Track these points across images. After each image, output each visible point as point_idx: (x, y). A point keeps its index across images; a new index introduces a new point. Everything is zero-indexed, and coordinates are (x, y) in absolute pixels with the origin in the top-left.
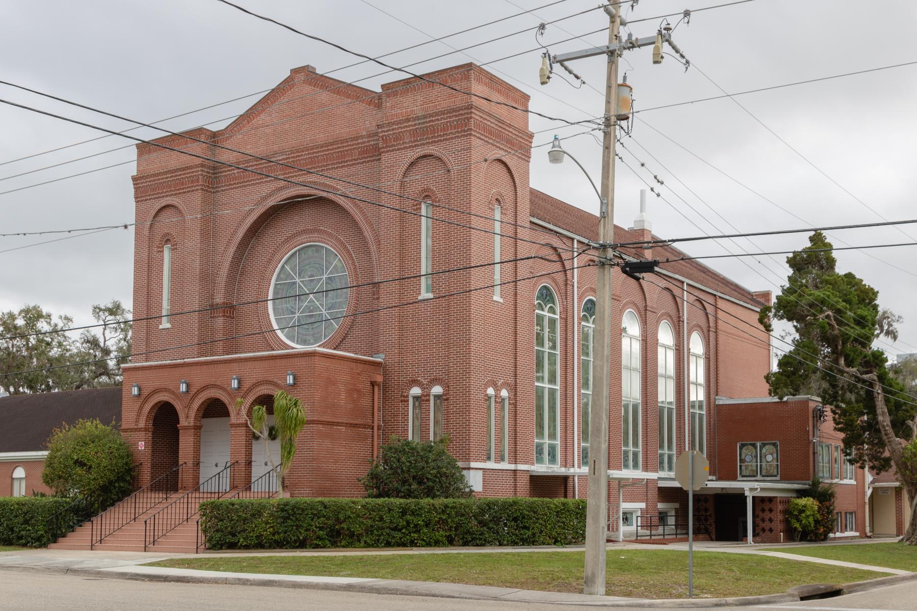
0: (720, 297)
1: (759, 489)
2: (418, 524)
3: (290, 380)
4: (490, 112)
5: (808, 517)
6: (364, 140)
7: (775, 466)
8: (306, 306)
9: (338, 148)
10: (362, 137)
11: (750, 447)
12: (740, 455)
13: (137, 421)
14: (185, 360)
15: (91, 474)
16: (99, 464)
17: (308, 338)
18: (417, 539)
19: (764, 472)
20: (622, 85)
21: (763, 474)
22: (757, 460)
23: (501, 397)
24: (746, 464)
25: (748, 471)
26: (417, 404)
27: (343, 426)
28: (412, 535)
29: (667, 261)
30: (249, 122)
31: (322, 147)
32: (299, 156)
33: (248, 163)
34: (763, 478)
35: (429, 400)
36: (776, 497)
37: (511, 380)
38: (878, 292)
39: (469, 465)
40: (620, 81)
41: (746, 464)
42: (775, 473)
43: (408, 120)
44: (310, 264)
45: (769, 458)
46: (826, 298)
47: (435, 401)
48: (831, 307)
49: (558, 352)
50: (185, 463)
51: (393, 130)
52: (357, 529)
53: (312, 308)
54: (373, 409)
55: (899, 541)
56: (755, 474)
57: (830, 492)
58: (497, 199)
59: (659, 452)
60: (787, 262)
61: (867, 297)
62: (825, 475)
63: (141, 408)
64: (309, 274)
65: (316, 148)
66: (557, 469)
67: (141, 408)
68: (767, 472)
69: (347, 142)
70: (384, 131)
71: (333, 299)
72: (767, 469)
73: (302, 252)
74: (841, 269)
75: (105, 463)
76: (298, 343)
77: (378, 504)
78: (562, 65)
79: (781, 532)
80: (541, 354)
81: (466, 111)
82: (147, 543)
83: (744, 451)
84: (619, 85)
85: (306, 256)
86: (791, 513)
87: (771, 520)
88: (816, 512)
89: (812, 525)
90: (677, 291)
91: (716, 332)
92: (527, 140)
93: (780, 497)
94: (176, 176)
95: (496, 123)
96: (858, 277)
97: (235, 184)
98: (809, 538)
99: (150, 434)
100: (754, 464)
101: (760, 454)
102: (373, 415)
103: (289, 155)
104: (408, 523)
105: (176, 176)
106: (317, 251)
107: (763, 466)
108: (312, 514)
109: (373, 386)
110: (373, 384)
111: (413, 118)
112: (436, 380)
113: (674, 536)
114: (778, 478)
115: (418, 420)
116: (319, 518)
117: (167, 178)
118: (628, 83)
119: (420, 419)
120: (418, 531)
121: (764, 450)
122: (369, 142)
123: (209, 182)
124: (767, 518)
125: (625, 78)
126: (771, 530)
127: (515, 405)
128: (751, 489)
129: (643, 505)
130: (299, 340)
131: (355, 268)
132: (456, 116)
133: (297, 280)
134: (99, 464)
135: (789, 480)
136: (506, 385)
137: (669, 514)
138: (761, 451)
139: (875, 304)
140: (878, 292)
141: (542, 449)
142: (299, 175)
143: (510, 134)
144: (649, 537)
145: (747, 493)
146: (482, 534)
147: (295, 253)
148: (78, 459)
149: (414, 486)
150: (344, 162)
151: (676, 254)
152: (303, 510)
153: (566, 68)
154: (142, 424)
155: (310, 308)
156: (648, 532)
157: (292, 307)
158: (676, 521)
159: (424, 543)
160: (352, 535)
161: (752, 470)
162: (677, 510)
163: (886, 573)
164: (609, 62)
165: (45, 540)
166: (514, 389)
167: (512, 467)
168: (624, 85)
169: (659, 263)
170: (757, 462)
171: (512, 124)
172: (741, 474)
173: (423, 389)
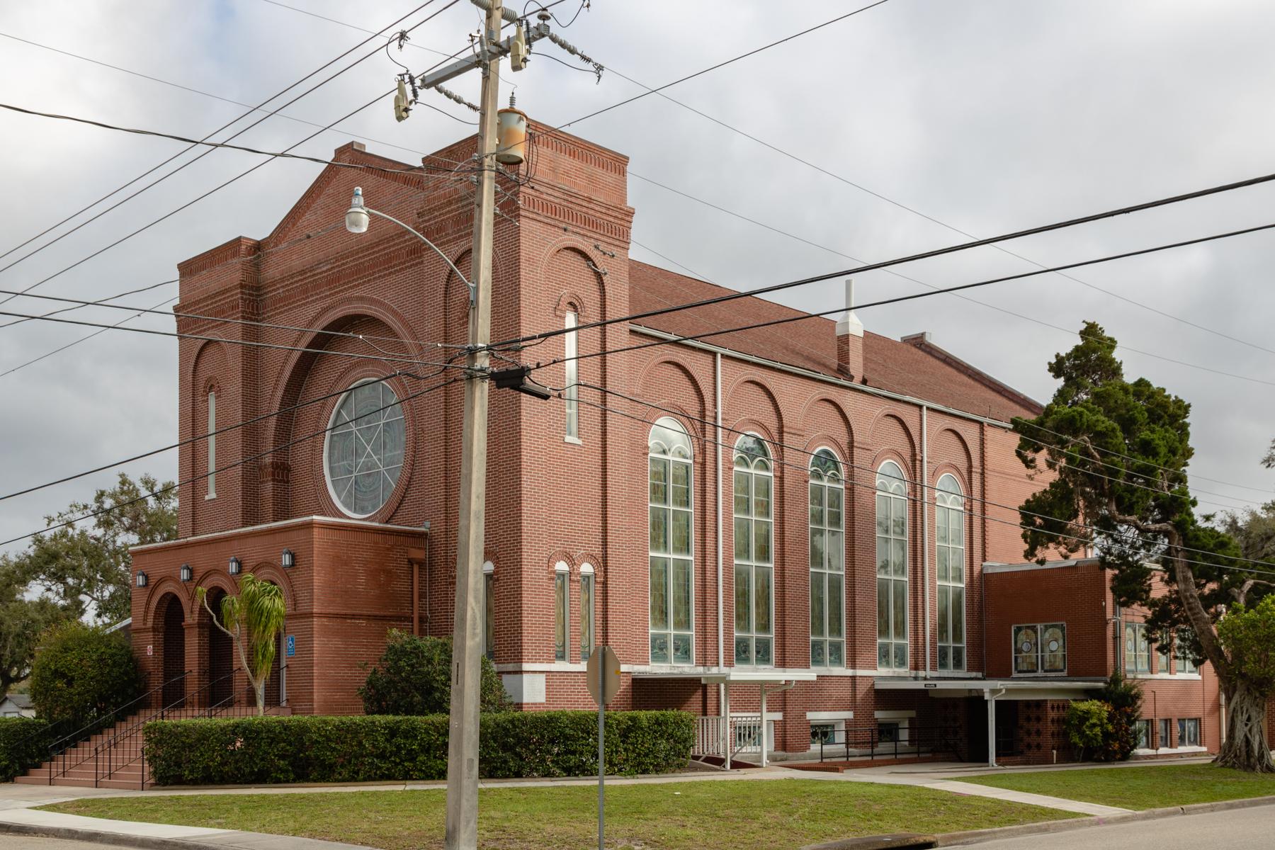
0: (989, 425)
1: (1004, 691)
2: (412, 750)
3: (286, 560)
4: (552, 183)
5: (1094, 725)
9: (384, 249)
11: (1030, 632)
13: (145, 620)
14: (188, 539)
15: (72, 687)
16: (84, 675)
17: (366, 504)
18: (412, 770)
19: (1047, 666)
20: (506, 111)
22: (1037, 649)
23: (579, 574)
24: (1024, 654)
27: (363, 619)
28: (406, 764)
29: (538, 366)
30: (294, 225)
31: (367, 250)
32: (343, 264)
33: (292, 278)
34: (1021, 675)
36: (1046, 701)
37: (597, 551)
38: (1189, 406)
39: (521, 667)
40: (503, 104)
41: (1024, 654)
42: (1062, 667)
43: (450, 203)
45: (1054, 646)
46: (1078, 417)
48: (1089, 429)
50: (191, 671)
51: (435, 218)
52: (329, 756)
53: (370, 464)
54: (412, 594)
55: (1213, 762)
56: (1035, 669)
57: (1133, 692)
59: (879, 641)
60: (1050, 370)
61: (1166, 413)
62: (1139, 667)
63: (148, 603)
65: (362, 252)
66: (689, 669)
67: (148, 603)
69: (394, 239)
70: (425, 221)
71: (391, 451)
72: (1050, 662)
74: (1129, 377)
75: (92, 672)
76: (355, 512)
77: (355, 723)
78: (440, 90)
79: (1054, 749)
80: (661, 513)
82: (100, 776)
83: (1022, 636)
84: (501, 113)
86: (1072, 722)
87: (1038, 733)
88: (1105, 721)
89: (1099, 739)
90: (909, 416)
91: (983, 474)
92: (622, 219)
93: (1050, 700)
94: (216, 302)
95: (565, 197)
96: (1155, 385)
97: (280, 307)
98: (1095, 757)
99: (161, 636)
100: (1034, 655)
102: (413, 603)
103: (334, 263)
104: (399, 748)
105: (216, 302)
107: (1045, 658)
108: (268, 737)
109: (412, 565)
110: (411, 562)
111: (454, 199)
113: (916, 756)
116: (278, 743)
117: (207, 305)
118: (517, 107)
120: (413, 760)
121: (1047, 635)
123: (253, 307)
125: (512, 100)
126: (1038, 746)
127: (605, 584)
128: (994, 691)
129: (849, 715)
130: (357, 507)
133: (354, 429)
134: (84, 675)
136: (590, 557)
137: (900, 726)
139: (1184, 423)
140: (1189, 406)
142: (345, 289)
143: (591, 212)
145: (987, 697)
146: (506, 762)
148: (56, 670)
149: (418, 698)
150: (392, 267)
151: (963, 369)
152: (258, 733)
153: (449, 95)
154: (150, 624)
157: (349, 465)
158: (911, 735)
159: (422, 775)
160: (322, 764)
161: (1032, 663)
162: (911, 720)
163: (1074, 813)
164: (483, 78)
165: (10, 772)
166: (604, 562)
168: (511, 111)
169: (530, 370)
170: (1037, 652)
171: (593, 197)
172: (1016, 668)
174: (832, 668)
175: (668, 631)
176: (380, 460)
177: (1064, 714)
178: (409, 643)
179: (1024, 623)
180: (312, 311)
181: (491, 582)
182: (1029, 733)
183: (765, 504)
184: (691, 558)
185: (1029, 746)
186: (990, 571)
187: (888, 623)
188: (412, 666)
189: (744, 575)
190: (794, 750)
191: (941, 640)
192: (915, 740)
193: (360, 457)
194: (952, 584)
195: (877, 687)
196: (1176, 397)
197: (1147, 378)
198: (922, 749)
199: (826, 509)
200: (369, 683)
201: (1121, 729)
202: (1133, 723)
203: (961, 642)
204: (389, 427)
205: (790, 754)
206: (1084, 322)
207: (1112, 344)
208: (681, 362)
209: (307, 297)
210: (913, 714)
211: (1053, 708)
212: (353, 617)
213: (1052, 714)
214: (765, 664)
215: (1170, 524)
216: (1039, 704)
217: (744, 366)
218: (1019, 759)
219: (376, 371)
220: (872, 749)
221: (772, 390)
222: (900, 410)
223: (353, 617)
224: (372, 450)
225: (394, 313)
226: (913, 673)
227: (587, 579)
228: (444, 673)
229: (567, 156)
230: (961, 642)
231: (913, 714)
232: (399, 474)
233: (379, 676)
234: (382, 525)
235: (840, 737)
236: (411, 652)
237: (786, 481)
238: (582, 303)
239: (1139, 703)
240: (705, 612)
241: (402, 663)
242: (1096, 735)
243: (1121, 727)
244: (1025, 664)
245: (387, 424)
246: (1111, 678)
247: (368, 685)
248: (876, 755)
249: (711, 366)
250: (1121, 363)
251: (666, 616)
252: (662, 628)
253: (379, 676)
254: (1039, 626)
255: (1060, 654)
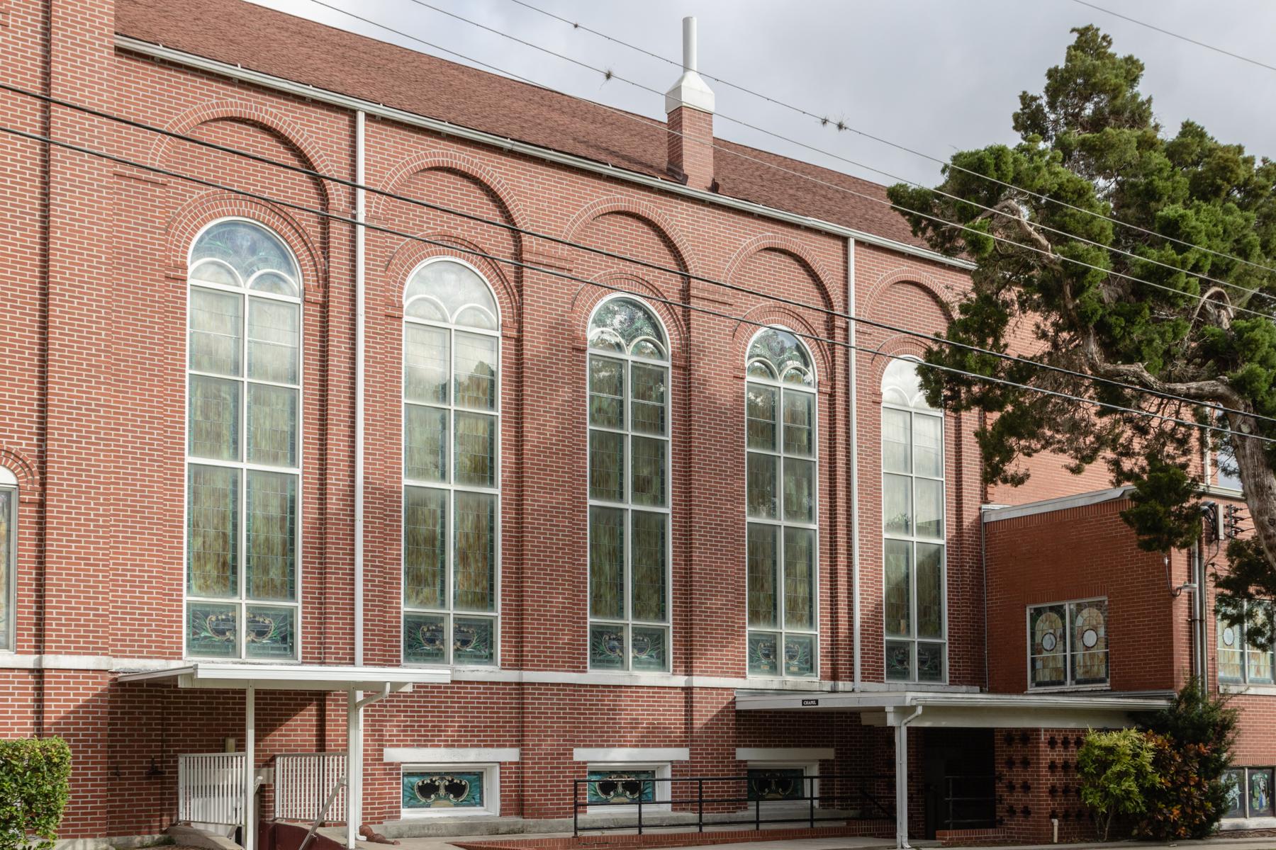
1: (919, 711)
5: (1121, 776)
7: (1102, 656)
11: (1054, 616)
12: (1033, 635)
19: (1080, 674)
21: (1078, 677)
24: (1045, 654)
25: (1047, 672)
34: (1041, 689)
36: (1038, 730)
41: (1045, 654)
42: (1103, 675)
45: (1090, 638)
49: (668, 437)
62: (1252, 675)
68: (1087, 672)
72: (1085, 666)
83: (1042, 625)
87: (1026, 787)
90: (823, 255)
93: (1046, 730)
98: (1135, 832)
100: (1060, 655)
101: (1072, 629)
113: (807, 825)
114: (1106, 686)
124: (1018, 782)
126: (1026, 812)
128: (904, 711)
129: (682, 754)
135: (1130, 690)
138: (1072, 622)
144: (695, 829)
156: (691, 816)
158: (823, 788)
161: (1056, 669)
162: (824, 764)
167: (512, 676)
172: (1033, 679)
174: (637, 673)
175: (235, 600)
177: (1074, 754)
179: (1044, 602)
182: (1011, 787)
183: (486, 384)
184: (298, 471)
185: (1011, 811)
186: (993, 518)
187: (775, 600)
189: (432, 506)
190: (540, 813)
191: (893, 629)
192: (833, 799)
194: (916, 539)
195: (739, 707)
196: (1264, 161)
197: (1199, 123)
198: (707, 816)
199: (629, 398)
201: (1186, 784)
202: (1217, 772)
203: (940, 636)
205: (531, 821)
206: (1073, 30)
207: (1132, 70)
208: (268, 120)
210: (829, 753)
211: (1052, 743)
213: (1048, 755)
214: (486, 663)
215: (1223, 382)
216: (1027, 736)
217: (429, 140)
218: (990, 833)
220: (701, 814)
221: (495, 185)
222: (796, 241)
226: (828, 685)
230: (940, 636)
231: (829, 753)
235: (664, 791)
237: (527, 345)
239: (1230, 735)
240: (323, 566)
242: (1128, 792)
243: (1187, 779)
244: (1047, 672)
246: (1183, 692)
248: (707, 824)
249: (345, 134)
250: (1149, 101)
252: (224, 595)
254: (1069, 606)
255: (1101, 651)
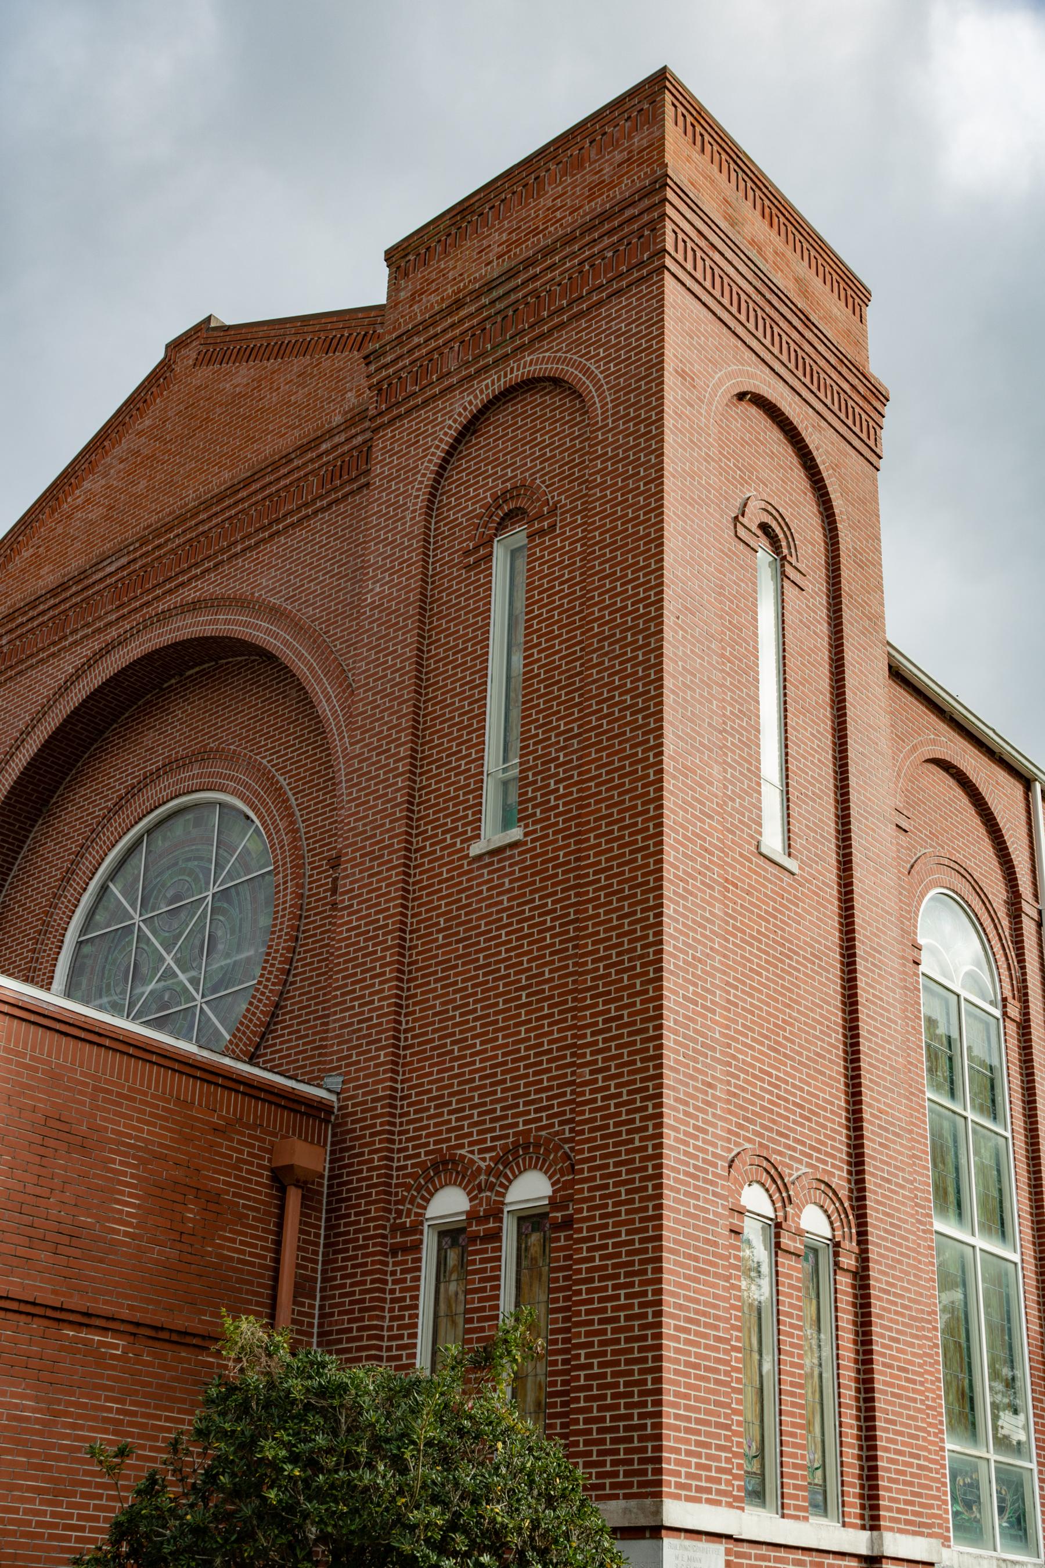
6: (337, 440)
8: (151, 992)
9: (263, 488)
10: (330, 433)
26: (453, 1257)
30: (53, 511)
31: (220, 501)
35: (495, 1236)
39: (658, 1512)
44: (176, 864)
47: (521, 1236)
58: (764, 527)
64: (170, 894)
71: (228, 955)
73: (157, 835)
81: (646, 202)
85: (167, 844)
103: (135, 550)
106: (197, 823)
109: (283, 1190)
112: (526, 1148)
115: (454, 1323)
119: (460, 1320)
122: (348, 440)
127: (861, 1278)
131: (295, 839)
132: (610, 233)
141: (975, 1486)
147: (137, 843)
155: (161, 997)
173: (474, 1192)
176: (194, 981)
178: (301, 1373)
180: (68, 664)
181: (535, 1238)
188: (312, 1464)
193: (145, 982)
200: (121, 1530)
204: (229, 901)
209: (64, 638)
212: (86, 1319)
219: (210, 775)
223: (86, 1319)
224: (177, 961)
225: (275, 613)
227: (811, 1256)
228: (435, 1500)
229: (522, 700)
232: (245, 1006)
233: (164, 1502)
234: (205, 1054)
236: (308, 1407)
238: (790, 536)
241: (270, 1450)
245: (224, 895)
247: (116, 1543)
251: (972, 1409)
253: (164, 1502)
